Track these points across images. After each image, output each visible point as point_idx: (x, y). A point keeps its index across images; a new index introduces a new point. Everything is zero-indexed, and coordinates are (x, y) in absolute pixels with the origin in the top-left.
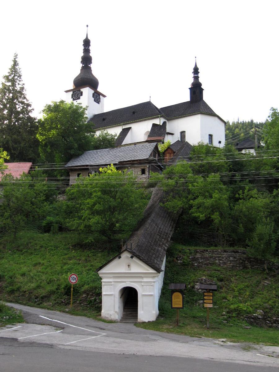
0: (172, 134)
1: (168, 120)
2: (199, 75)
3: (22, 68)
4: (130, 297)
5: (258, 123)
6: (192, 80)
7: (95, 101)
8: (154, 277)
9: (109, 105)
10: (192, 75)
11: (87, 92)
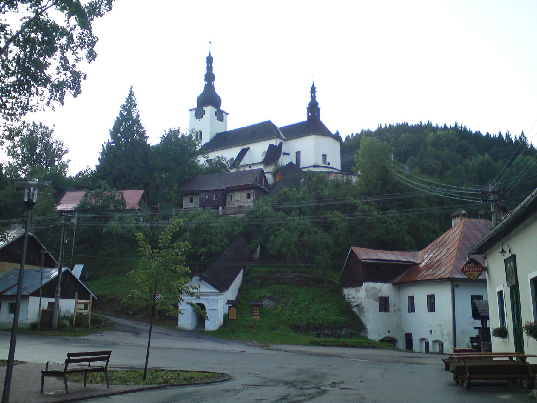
0: (289, 154)
1: (285, 140)
2: (316, 94)
3: (138, 98)
5: (414, 125)
6: (309, 100)
7: (217, 119)
8: (217, 295)
9: (233, 124)
11: (209, 110)
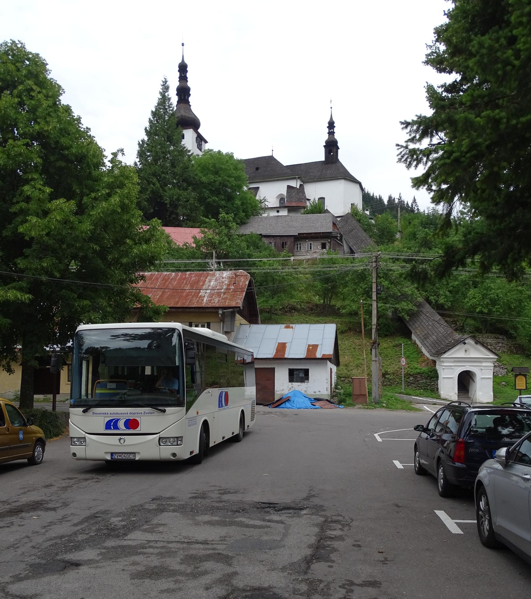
2: (335, 130)
4: (465, 380)
6: (326, 137)
10: (327, 130)
